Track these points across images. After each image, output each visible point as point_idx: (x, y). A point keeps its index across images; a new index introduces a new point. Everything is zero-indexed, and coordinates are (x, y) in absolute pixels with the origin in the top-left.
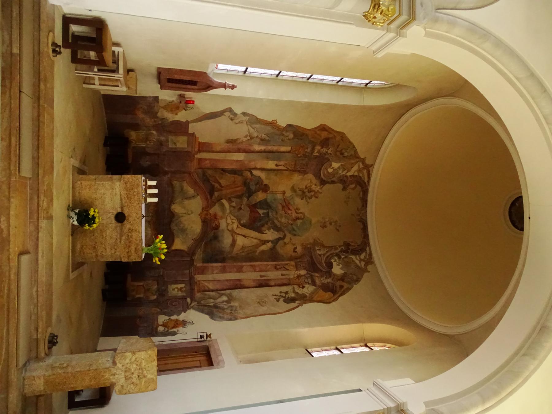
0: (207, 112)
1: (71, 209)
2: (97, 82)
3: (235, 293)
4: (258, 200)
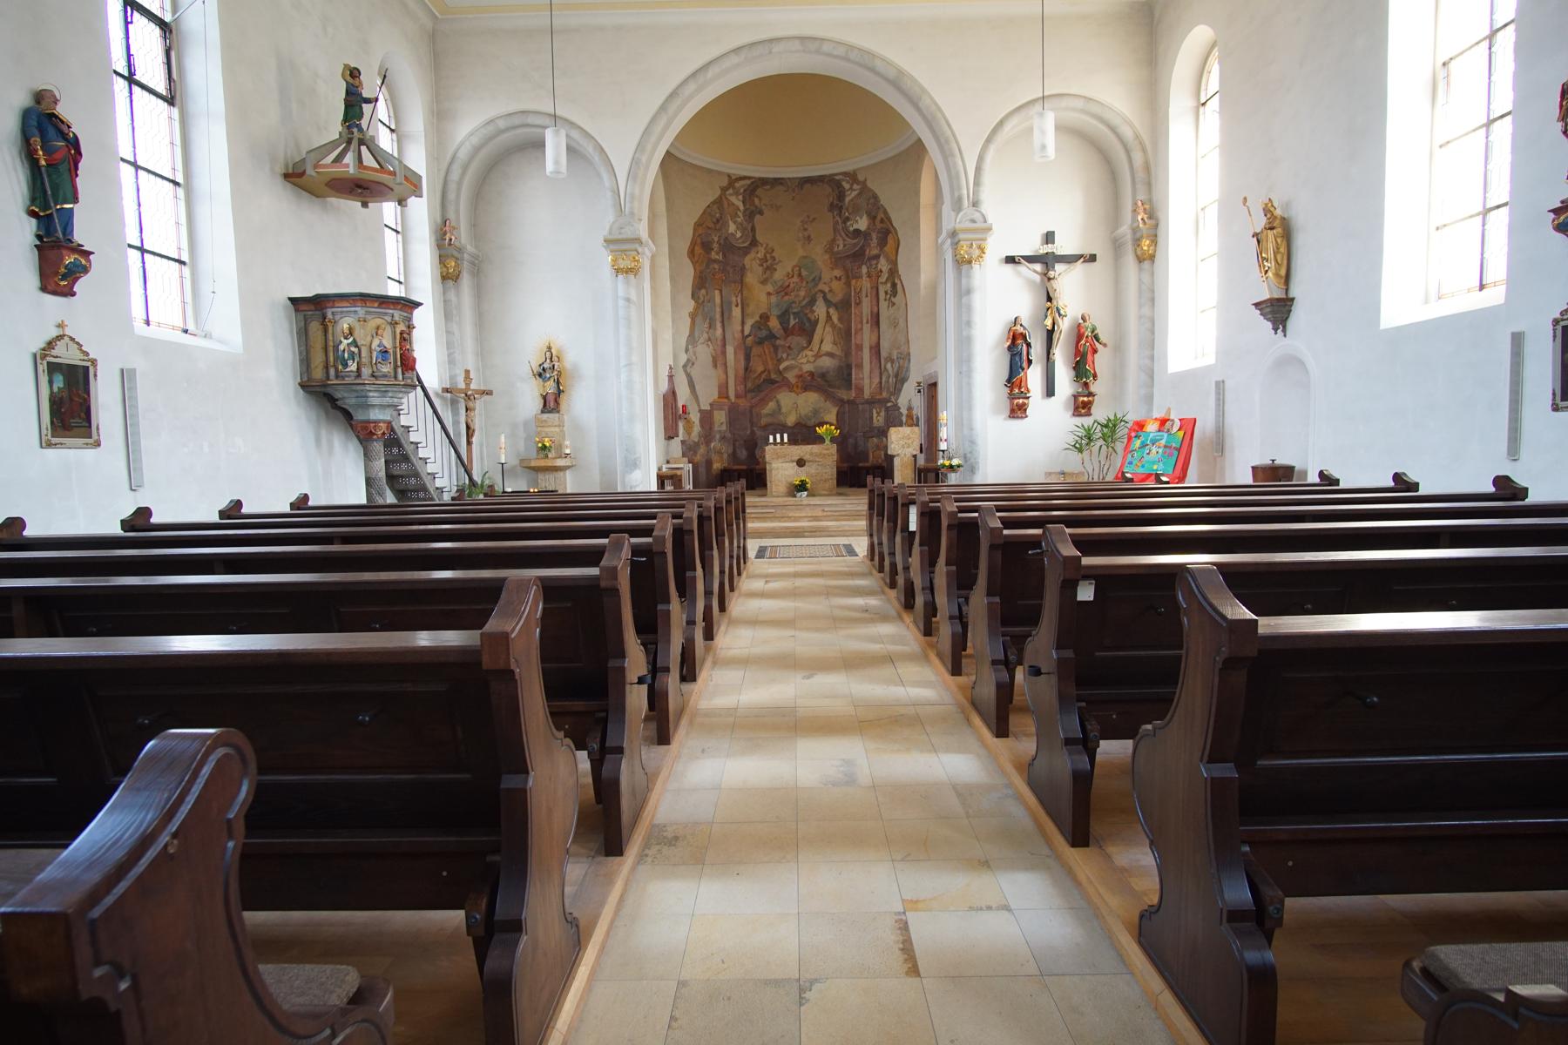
3: (884, 354)
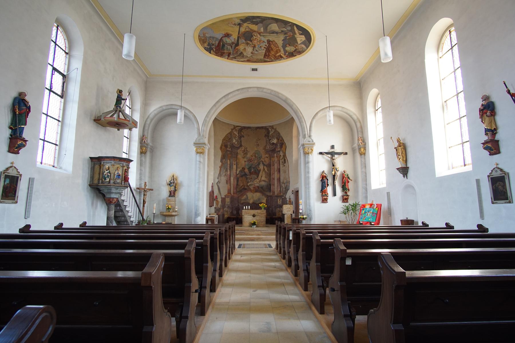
3: (281, 181)
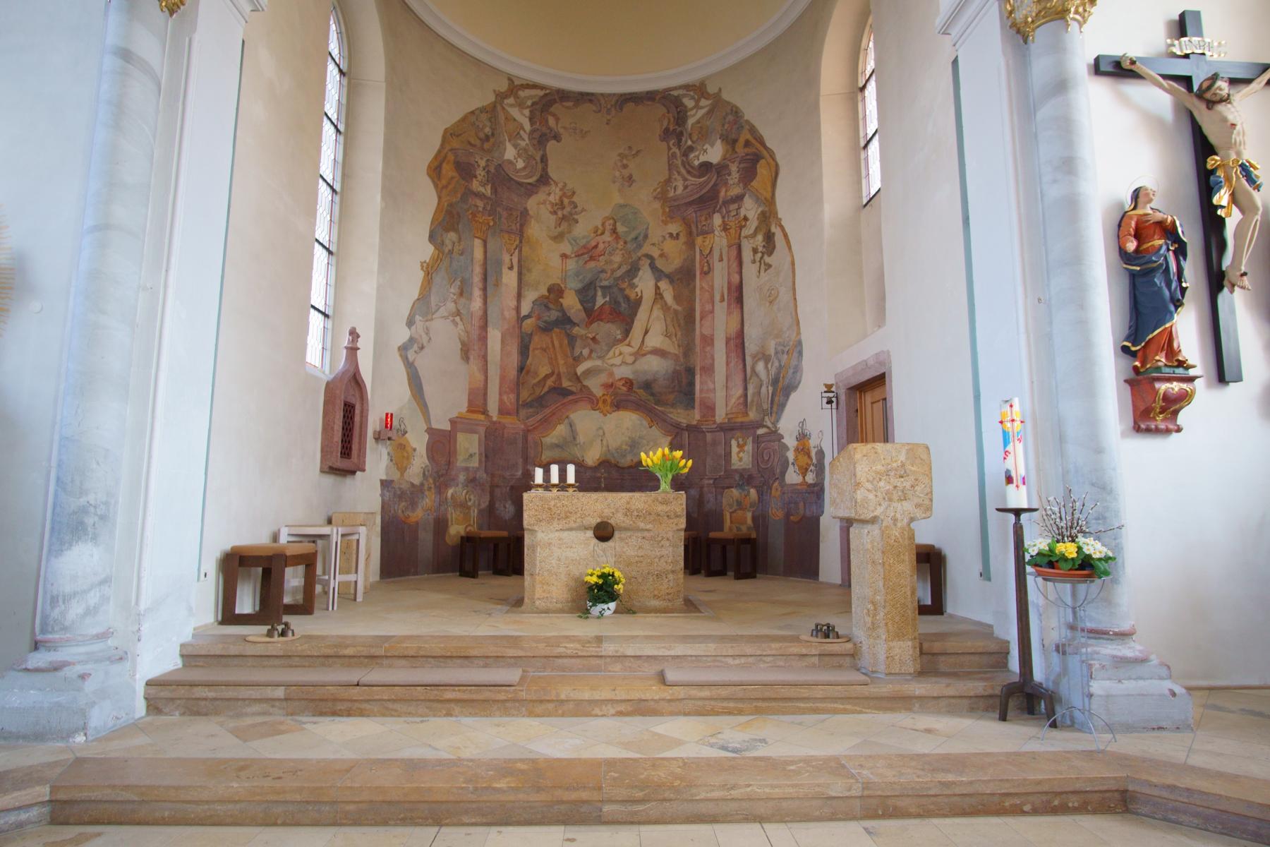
0: (409, 392)
1: (585, 613)
2: (352, 577)
3: (751, 347)
4: (579, 306)
